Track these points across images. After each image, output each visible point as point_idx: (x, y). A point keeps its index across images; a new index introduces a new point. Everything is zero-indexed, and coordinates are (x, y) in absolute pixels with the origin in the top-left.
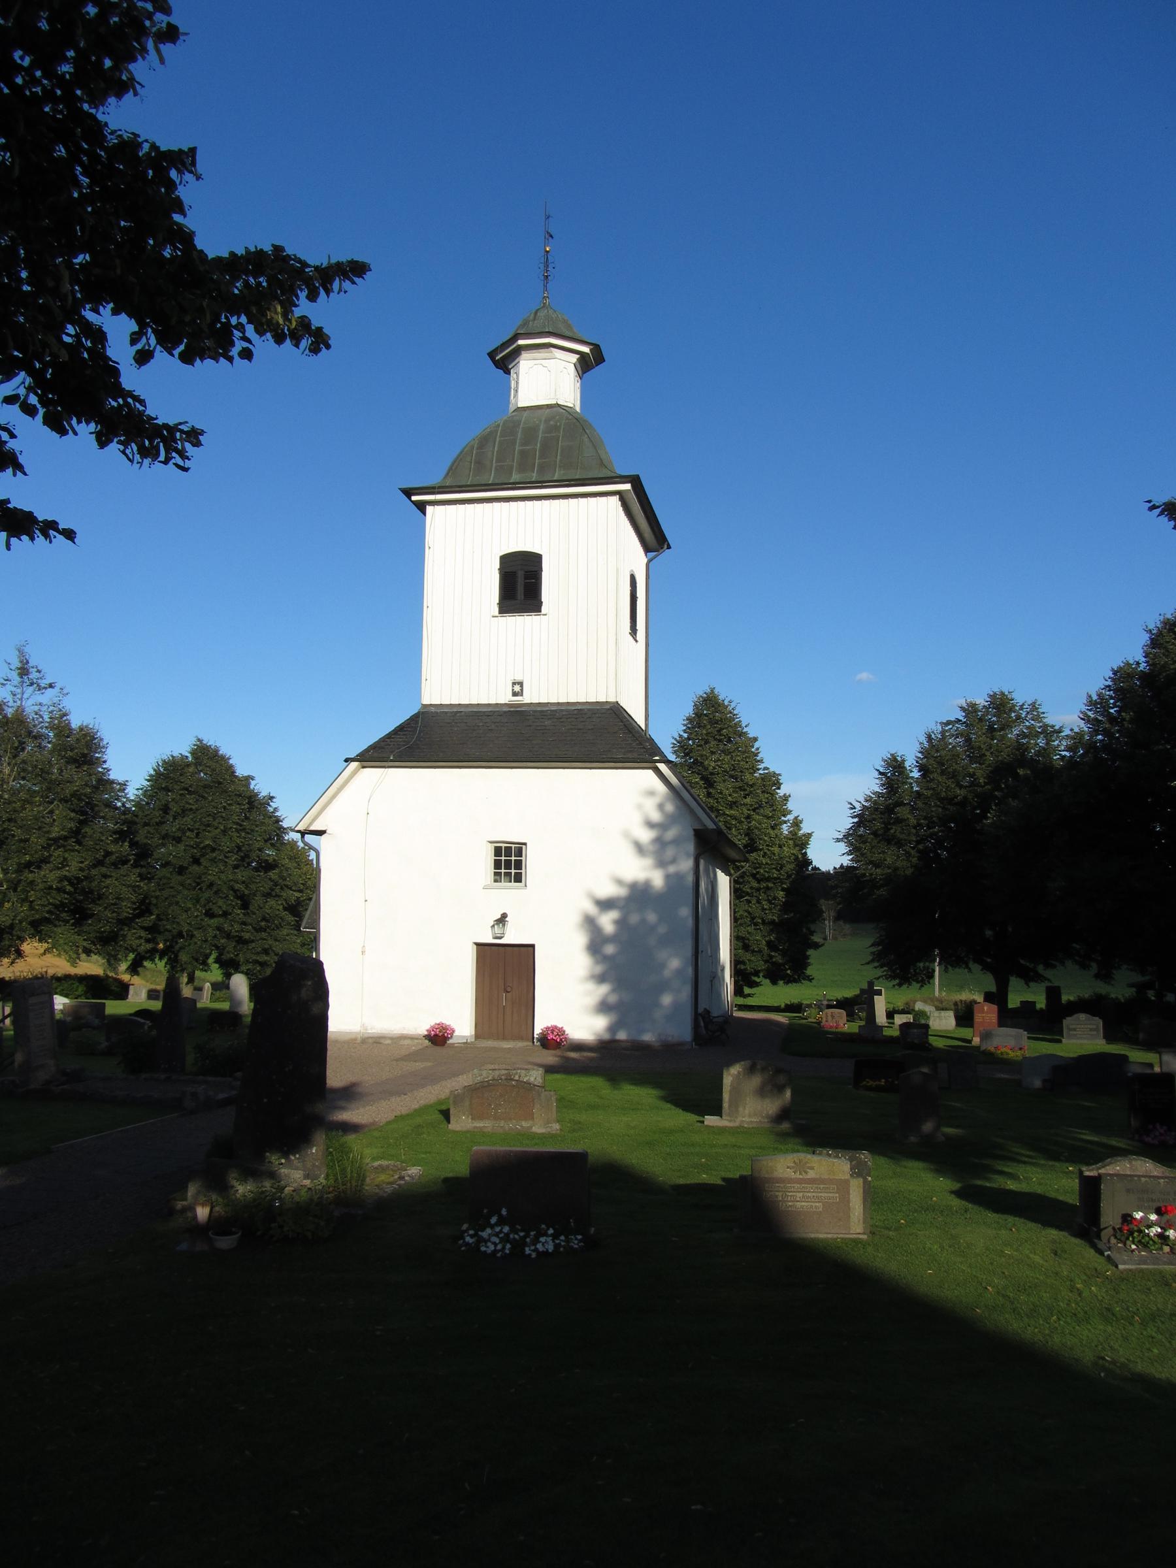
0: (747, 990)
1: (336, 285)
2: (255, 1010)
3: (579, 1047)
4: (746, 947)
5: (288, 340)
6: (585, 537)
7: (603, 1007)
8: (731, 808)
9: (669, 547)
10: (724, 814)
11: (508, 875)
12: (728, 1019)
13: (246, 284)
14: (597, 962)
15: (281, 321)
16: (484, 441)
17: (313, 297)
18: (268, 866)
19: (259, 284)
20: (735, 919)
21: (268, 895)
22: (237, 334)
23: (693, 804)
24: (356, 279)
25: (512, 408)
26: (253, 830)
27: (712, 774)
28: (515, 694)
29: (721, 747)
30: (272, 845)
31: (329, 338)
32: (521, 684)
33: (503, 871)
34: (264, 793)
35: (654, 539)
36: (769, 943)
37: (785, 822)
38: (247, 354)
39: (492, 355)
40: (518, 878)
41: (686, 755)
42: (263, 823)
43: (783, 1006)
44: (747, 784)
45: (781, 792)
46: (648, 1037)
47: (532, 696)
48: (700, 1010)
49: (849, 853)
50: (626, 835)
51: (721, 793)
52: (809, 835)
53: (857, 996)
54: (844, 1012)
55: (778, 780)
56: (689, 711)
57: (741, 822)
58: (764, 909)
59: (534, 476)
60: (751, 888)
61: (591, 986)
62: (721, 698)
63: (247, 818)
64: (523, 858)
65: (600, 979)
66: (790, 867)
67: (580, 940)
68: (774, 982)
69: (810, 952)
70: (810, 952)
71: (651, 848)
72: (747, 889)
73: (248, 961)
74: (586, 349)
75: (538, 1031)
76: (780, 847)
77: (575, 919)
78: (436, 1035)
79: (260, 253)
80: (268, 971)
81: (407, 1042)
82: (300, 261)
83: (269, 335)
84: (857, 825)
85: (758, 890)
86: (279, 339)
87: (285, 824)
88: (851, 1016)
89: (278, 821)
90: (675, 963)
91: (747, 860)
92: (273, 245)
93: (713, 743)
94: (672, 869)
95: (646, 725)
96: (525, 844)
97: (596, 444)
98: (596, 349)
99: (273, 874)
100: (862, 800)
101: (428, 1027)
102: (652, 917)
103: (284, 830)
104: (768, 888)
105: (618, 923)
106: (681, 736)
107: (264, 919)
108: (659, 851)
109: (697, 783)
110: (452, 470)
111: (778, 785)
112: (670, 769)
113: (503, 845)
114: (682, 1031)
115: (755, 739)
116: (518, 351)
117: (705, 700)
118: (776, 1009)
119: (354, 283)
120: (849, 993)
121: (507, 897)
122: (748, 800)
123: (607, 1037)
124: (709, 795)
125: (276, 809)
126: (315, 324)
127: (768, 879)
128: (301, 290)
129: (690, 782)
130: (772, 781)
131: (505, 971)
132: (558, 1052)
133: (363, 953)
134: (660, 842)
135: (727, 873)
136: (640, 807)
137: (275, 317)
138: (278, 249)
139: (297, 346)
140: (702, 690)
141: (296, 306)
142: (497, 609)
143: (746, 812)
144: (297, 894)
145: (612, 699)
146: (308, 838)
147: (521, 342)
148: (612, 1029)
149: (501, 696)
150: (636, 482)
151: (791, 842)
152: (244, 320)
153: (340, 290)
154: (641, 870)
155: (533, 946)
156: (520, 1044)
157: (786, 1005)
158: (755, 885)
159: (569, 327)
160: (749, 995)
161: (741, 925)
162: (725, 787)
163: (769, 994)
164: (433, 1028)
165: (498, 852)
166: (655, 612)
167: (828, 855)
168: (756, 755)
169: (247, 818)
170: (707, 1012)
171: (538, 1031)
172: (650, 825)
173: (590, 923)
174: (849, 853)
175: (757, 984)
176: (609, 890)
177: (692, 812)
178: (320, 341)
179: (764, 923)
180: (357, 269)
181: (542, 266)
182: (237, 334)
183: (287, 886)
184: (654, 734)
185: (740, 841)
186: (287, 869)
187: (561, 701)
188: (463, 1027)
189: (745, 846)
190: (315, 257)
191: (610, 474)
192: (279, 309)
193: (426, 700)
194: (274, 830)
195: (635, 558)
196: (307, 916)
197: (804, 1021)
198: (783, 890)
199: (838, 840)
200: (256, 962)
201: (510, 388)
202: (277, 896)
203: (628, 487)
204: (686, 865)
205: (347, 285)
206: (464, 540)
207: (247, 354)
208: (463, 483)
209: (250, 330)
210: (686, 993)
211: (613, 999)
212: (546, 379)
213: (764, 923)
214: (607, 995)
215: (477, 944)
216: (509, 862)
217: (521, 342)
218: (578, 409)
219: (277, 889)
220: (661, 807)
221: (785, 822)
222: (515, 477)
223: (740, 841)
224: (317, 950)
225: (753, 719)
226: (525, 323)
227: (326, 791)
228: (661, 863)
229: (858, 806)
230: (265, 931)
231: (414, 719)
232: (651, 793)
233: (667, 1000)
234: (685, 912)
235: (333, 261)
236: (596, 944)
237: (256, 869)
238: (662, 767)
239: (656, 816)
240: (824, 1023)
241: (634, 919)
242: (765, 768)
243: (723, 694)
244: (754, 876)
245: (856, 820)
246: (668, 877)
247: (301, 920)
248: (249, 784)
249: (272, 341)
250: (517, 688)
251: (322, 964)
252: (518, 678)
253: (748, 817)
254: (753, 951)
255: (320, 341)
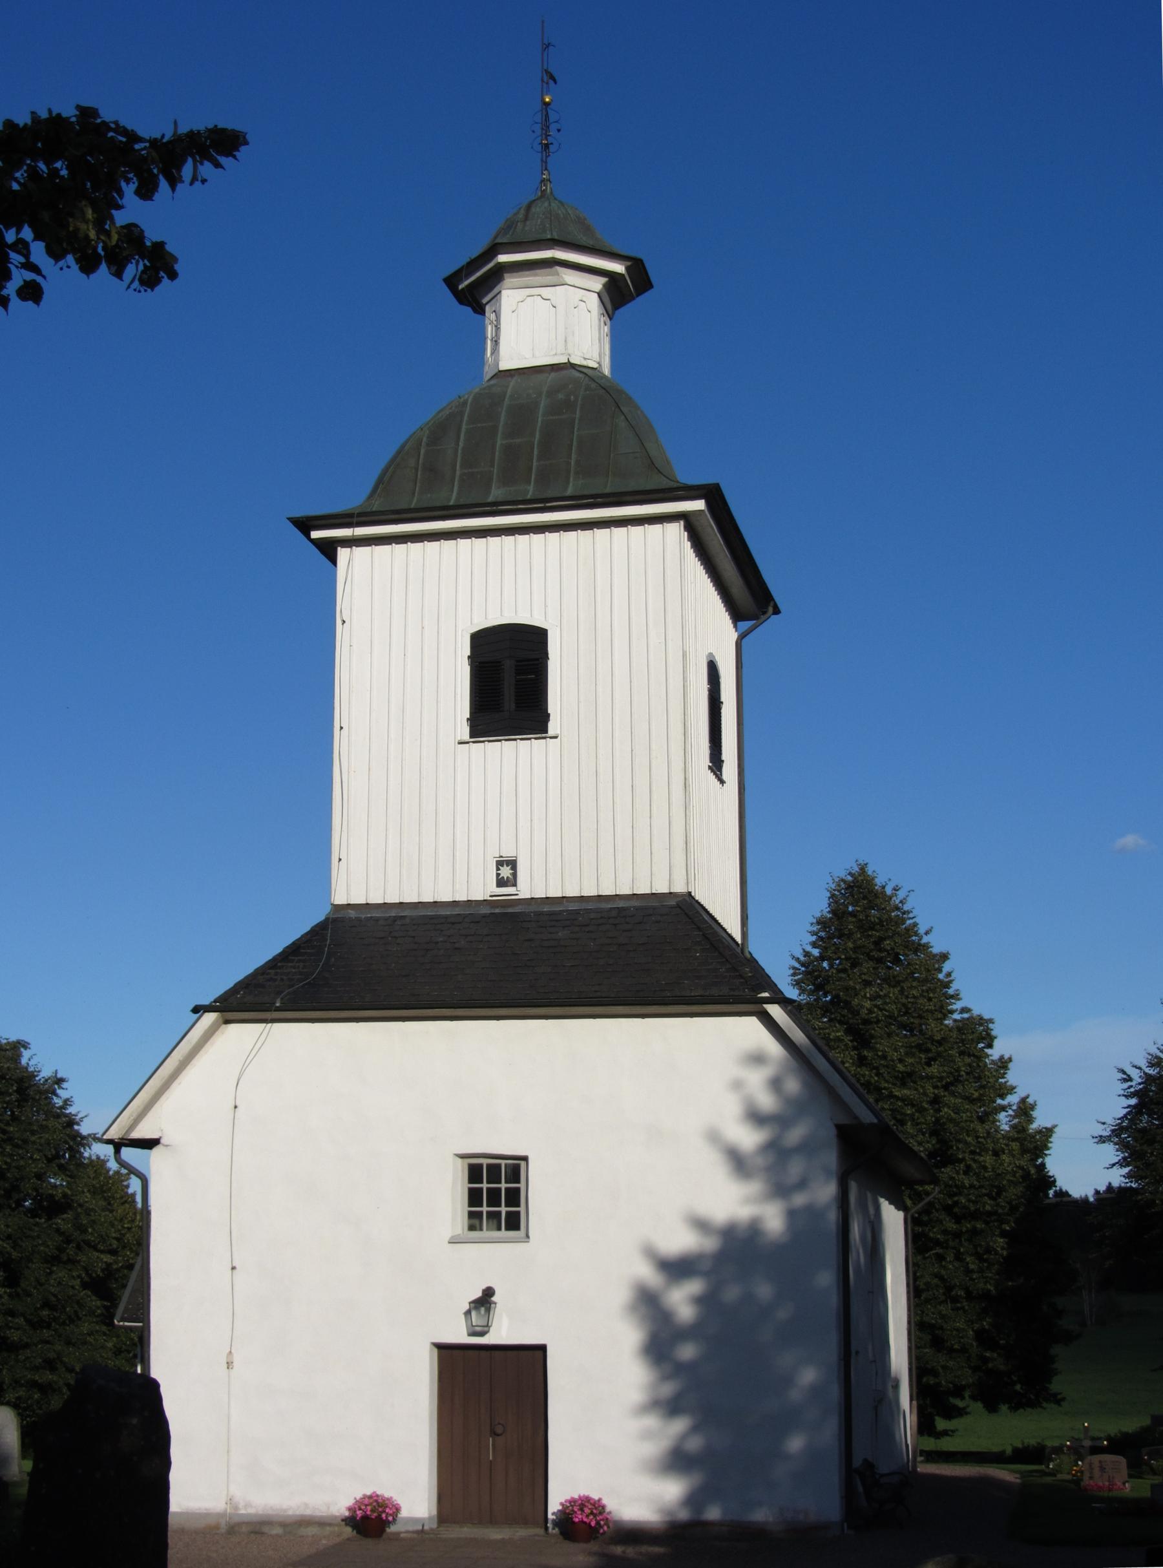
0: (941, 1424)
1: (187, 170)
2: (32, 1475)
3: (633, 1534)
4: (938, 1343)
5: (104, 267)
6: (625, 599)
7: (677, 1461)
8: (904, 1084)
9: (777, 611)
10: (891, 1095)
11: (494, 1216)
12: (907, 1479)
13: (33, 174)
14: (665, 1378)
15: (92, 234)
16: (440, 429)
17: (146, 191)
18: (53, 1206)
19: (54, 173)
20: (916, 1292)
21: (53, 1260)
22: (16, 258)
23: (835, 1079)
24: (222, 160)
25: (488, 372)
26: (25, 1141)
27: (866, 1022)
28: (501, 882)
29: (882, 972)
30: (62, 1168)
31: (176, 260)
32: (513, 864)
33: (485, 1209)
34: (46, 1073)
35: (749, 597)
36: (980, 1335)
37: (1003, 1108)
38: (32, 292)
39: (451, 282)
40: (514, 1222)
41: (819, 987)
42: (44, 1128)
43: (1009, 1451)
44: (931, 1039)
45: (995, 1053)
46: (761, 1515)
47: (533, 885)
48: (857, 1462)
49: (1122, 1163)
50: (714, 1137)
51: (884, 1057)
52: (1048, 1133)
53: (1145, 1430)
54: (1122, 1461)
55: (988, 1031)
56: (820, 906)
57: (921, 1110)
58: (968, 1272)
59: (531, 491)
60: (945, 1232)
61: (651, 1421)
62: (879, 881)
63: (14, 1118)
64: (522, 1185)
65: (671, 1407)
66: (1014, 1192)
67: (629, 1336)
68: (992, 1408)
69: (1057, 1350)
70: (1057, 1350)
71: (760, 1161)
72: (935, 1233)
73: (16, 1383)
74: (618, 267)
75: (554, 1506)
76: (996, 1154)
77: (620, 1295)
78: (365, 1518)
79: (57, 121)
80: (56, 1403)
81: (311, 1531)
82: (125, 132)
83: (70, 259)
84: (1135, 1113)
85: (957, 1235)
86: (88, 266)
87: (85, 1129)
88: (1136, 1469)
89: (71, 1122)
90: (808, 1376)
91: (935, 1181)
92: (78, 107)
93: (868, 965)
94: (799, 1200)
95: (744, 934)
96: (525, 1159)
97: (641, 431)
98: (637, 267)
99: (63, 1222)
100: (1143, 1063)
101: (350, 1502)
102: (764, 1291)
103: (81, 1141)
104: (974, 1232)
105: (700, 1301)
106: (807, 954)
107: (46, 1304)
108: (773, 1165)
109: (838, 1039)
110: (383, 483)
111: (990, 1041)
112: (790, 1014)
113: (485, 1162)
114: (823, 1503)
115: (944, 957)
116: (499, 273)
117: (850, 887)
118: (997, 1458)
119: (217, 165)
120: (1131, 1425)
121: (491, 1260)
122: (934, 1069)
123: (684, 1515)
124: (862, 1061)
125: (67, 1102)
126: (152, 235)
127: (975, 1216)
128: (128, 181)
129: (827, 1039)
130: (977, 1032)
131: (492, 1395)
132: (593, 1546)
133: (229, 1365)
134: (776, 1151)
135: (899, 1205)
136: (737, 1085)
137: (83, 226)
138: (87, 113)
139: (119, 274)
140: (843, 868)
141: (119, 207)
142: (467, 730)
143: (930, 1090)
144: (107, 1258)
145: (679, 888)
146: (127, 1153)
147: (503, 258)
148: (693, 1500)
149: (476, 885)
150: (713, 495)
151: (1015, 1146)
152: (27, 233)
153: (194, 179)
154: (732, 1201)
155: (542, 1349)
156: (521, 1532)
157: (1016, 1451)
158: (951, 1226)
159: (587, 229)
160: (945, 1433)
161: (927, 1301)
162: (891, 1046)
163: (983, 1429)
164: (360, 1504)
165: (474, 1173)
166: (757, 733)
167: (1084, 1167)
168: (947, 985)
169: (14, 1118)
170: (869, 1465)
171: (554, 1506)
172: (756, 1117)
173: (648, 1303)
174: (1122, 1163)
175: (961, 1412)
176: (680, 1240)
177: (831, 1092)
178: (158, 265)
179: (969, 1296)
180: (222, 143)
181: (538, 128)
182: (16, 258)
183: (88, 1243)
184: (759, 950)
185: (921, 1145)
186: (88, 1212)
187: (585, 894)
188: (416, 1500)
189: (932, 1155)
190: (150, 120)
191: (665, 483)
192: (89, 213)
193: (340, 897)
194: (66, 1136)
195: (715, 631)
196: (125, 1299)
197: (1049, 1479)
198: (1003, 1234)
199: (1102, 1140)
200: (33, 1384)
201: (485, 338)
202: (71, 1261)
203: (699, 505)
204: (825, 1192)
205: (206, 169)
206: (405, 608)
207: (32, 292)
208: (405, 506)
209: (38, 254)
210: (830, 1431)
211: (695, 1444)
212: (549, 322)
213: (969, 1296)
214: (684, 1437)
215: (441, 1348)
216: (495, 1193)
217: (503, 258)
218: (606, 371)
219: (71, 1250)
220: (775, 1084)
221: (1003, 1108)
222: (496, 493)
223: (921, 1145)
224: (145, 1360)
225: (940, 918)
226: (510, 225)
227: (160, 1070)
228: (779, 1190)
229: (1136, 1075)
230: (49, 1327)
231: (318, 931)
232: (757, 1059)
233: (796, 1444)
234: (826, 1279)
235: (183, 129)
236: (661, 1342)
237: (33, 1213)
238: (775, 1011)
239: (766, 1101)
240: (1086, 1481)
241: (732, 1294)
242: (964, 1010)
243: (884, 875)
244: (948, 1209)
245: (1133, 1101)
246: (792, 1215)
247: (115, 1306)
248: (20, 1055)
249: (75, 267)
250: (506, 872)
251: (155, 1385)
252: (508, 853)
253: (936, 1101)
254: (951, 1350)
255: (158, 265)
